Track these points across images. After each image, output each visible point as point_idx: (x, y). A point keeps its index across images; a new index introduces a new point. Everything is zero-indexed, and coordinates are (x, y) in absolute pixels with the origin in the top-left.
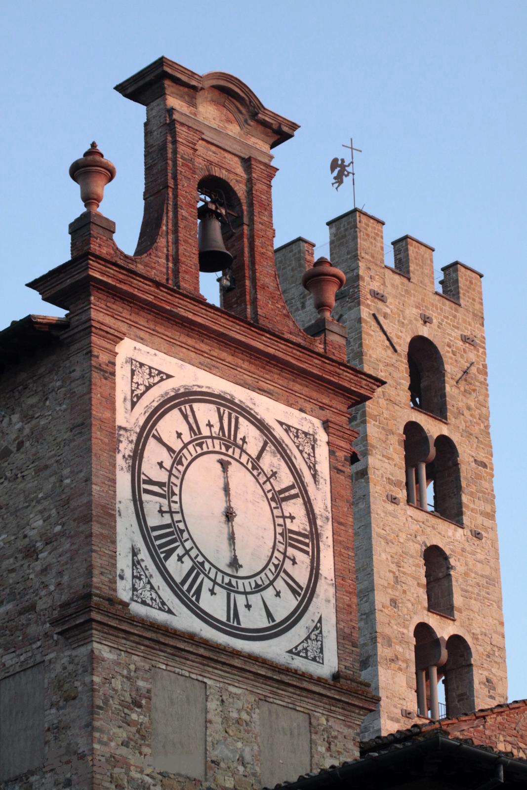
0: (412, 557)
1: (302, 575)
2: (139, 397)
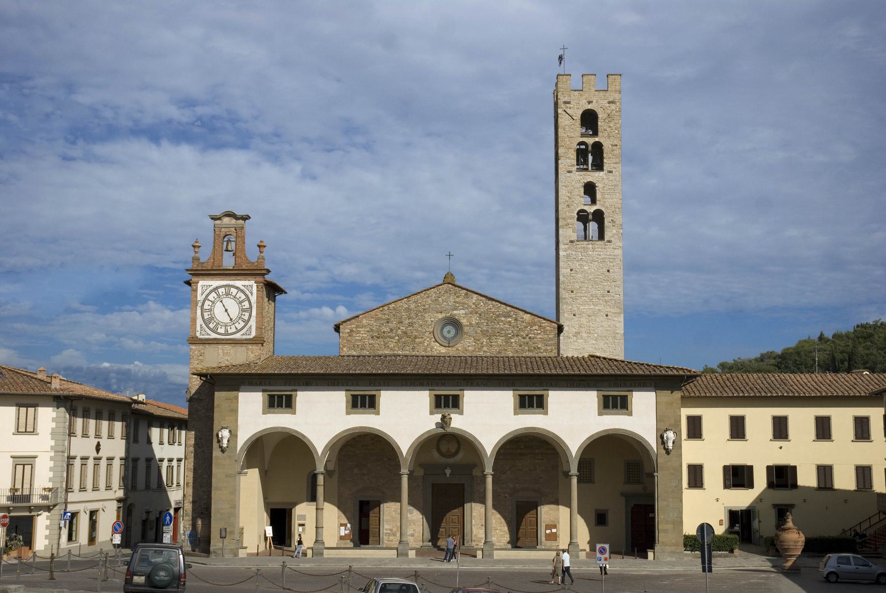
1: (246, 318)
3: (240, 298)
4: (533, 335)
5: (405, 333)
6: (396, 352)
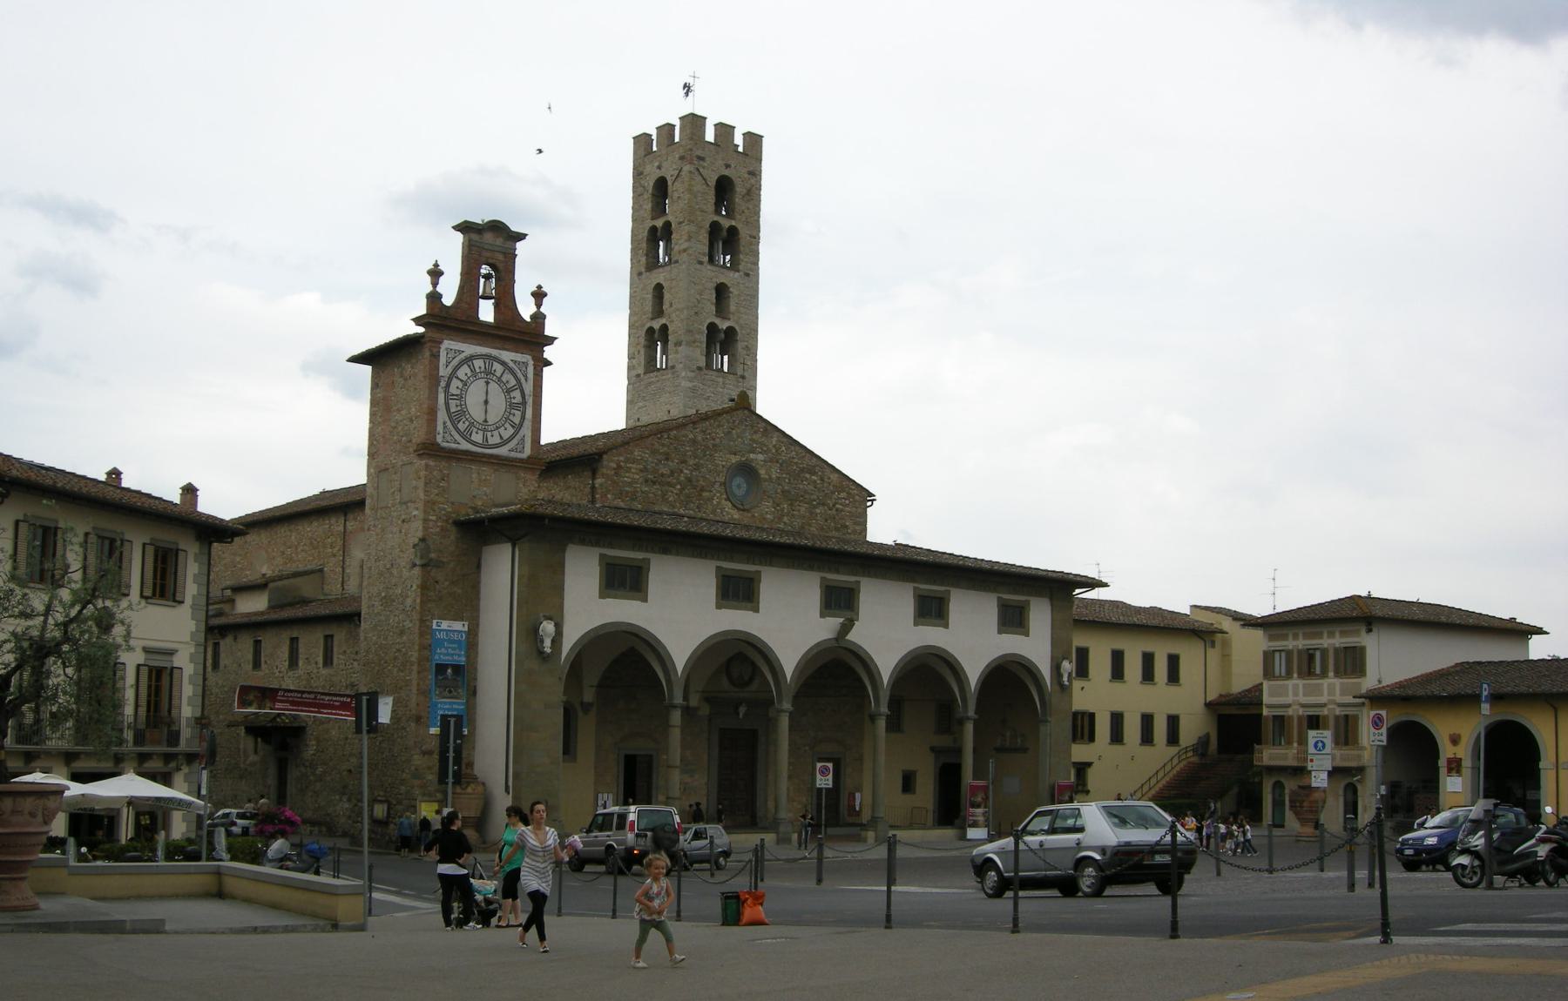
1: (517, 420)
3: (507, 382)
4: (841, 507)
5: (689, 480)
6: (676, 510)
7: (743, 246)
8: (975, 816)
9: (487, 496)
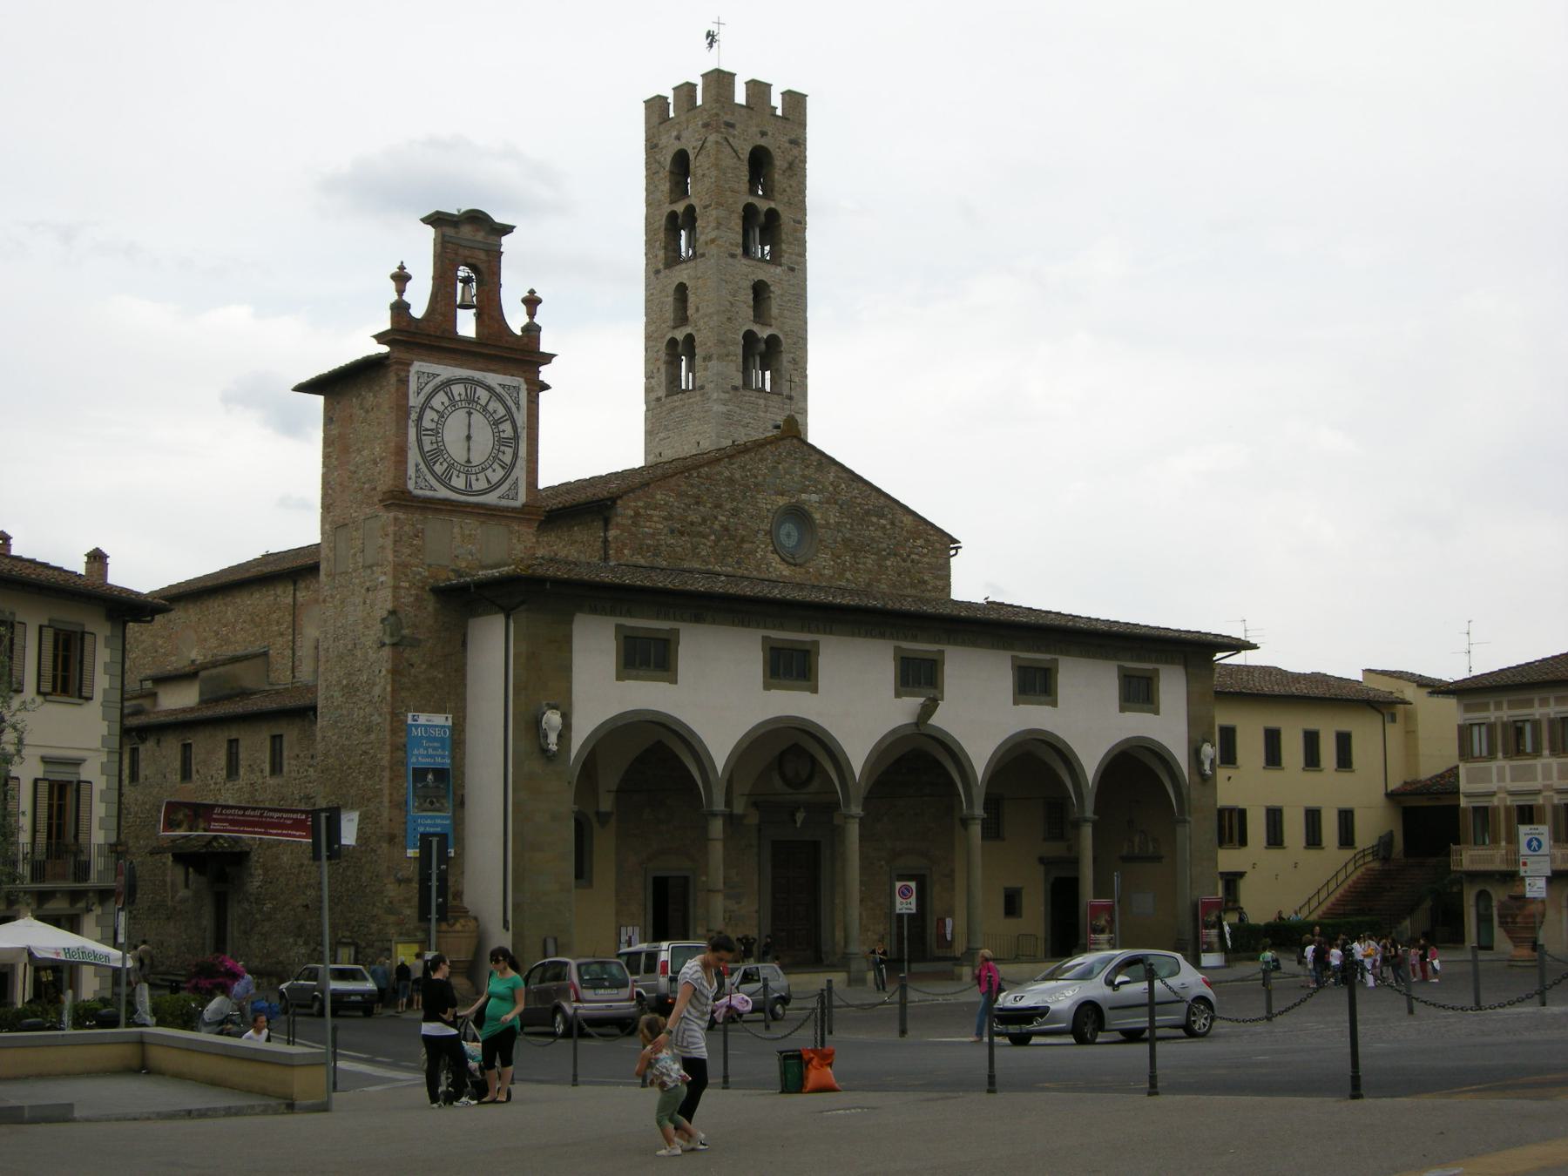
0: (744, 289)
1: (507, 459)
2: (421, 390)
3: (495, 412)
6: (711, 567)
7: (786, 234)
8: (1099, 944)
9: (472, 556)
